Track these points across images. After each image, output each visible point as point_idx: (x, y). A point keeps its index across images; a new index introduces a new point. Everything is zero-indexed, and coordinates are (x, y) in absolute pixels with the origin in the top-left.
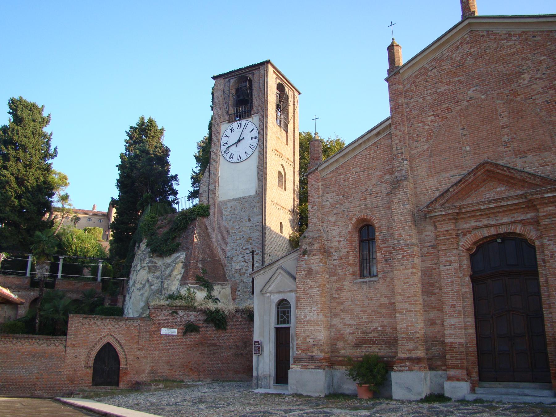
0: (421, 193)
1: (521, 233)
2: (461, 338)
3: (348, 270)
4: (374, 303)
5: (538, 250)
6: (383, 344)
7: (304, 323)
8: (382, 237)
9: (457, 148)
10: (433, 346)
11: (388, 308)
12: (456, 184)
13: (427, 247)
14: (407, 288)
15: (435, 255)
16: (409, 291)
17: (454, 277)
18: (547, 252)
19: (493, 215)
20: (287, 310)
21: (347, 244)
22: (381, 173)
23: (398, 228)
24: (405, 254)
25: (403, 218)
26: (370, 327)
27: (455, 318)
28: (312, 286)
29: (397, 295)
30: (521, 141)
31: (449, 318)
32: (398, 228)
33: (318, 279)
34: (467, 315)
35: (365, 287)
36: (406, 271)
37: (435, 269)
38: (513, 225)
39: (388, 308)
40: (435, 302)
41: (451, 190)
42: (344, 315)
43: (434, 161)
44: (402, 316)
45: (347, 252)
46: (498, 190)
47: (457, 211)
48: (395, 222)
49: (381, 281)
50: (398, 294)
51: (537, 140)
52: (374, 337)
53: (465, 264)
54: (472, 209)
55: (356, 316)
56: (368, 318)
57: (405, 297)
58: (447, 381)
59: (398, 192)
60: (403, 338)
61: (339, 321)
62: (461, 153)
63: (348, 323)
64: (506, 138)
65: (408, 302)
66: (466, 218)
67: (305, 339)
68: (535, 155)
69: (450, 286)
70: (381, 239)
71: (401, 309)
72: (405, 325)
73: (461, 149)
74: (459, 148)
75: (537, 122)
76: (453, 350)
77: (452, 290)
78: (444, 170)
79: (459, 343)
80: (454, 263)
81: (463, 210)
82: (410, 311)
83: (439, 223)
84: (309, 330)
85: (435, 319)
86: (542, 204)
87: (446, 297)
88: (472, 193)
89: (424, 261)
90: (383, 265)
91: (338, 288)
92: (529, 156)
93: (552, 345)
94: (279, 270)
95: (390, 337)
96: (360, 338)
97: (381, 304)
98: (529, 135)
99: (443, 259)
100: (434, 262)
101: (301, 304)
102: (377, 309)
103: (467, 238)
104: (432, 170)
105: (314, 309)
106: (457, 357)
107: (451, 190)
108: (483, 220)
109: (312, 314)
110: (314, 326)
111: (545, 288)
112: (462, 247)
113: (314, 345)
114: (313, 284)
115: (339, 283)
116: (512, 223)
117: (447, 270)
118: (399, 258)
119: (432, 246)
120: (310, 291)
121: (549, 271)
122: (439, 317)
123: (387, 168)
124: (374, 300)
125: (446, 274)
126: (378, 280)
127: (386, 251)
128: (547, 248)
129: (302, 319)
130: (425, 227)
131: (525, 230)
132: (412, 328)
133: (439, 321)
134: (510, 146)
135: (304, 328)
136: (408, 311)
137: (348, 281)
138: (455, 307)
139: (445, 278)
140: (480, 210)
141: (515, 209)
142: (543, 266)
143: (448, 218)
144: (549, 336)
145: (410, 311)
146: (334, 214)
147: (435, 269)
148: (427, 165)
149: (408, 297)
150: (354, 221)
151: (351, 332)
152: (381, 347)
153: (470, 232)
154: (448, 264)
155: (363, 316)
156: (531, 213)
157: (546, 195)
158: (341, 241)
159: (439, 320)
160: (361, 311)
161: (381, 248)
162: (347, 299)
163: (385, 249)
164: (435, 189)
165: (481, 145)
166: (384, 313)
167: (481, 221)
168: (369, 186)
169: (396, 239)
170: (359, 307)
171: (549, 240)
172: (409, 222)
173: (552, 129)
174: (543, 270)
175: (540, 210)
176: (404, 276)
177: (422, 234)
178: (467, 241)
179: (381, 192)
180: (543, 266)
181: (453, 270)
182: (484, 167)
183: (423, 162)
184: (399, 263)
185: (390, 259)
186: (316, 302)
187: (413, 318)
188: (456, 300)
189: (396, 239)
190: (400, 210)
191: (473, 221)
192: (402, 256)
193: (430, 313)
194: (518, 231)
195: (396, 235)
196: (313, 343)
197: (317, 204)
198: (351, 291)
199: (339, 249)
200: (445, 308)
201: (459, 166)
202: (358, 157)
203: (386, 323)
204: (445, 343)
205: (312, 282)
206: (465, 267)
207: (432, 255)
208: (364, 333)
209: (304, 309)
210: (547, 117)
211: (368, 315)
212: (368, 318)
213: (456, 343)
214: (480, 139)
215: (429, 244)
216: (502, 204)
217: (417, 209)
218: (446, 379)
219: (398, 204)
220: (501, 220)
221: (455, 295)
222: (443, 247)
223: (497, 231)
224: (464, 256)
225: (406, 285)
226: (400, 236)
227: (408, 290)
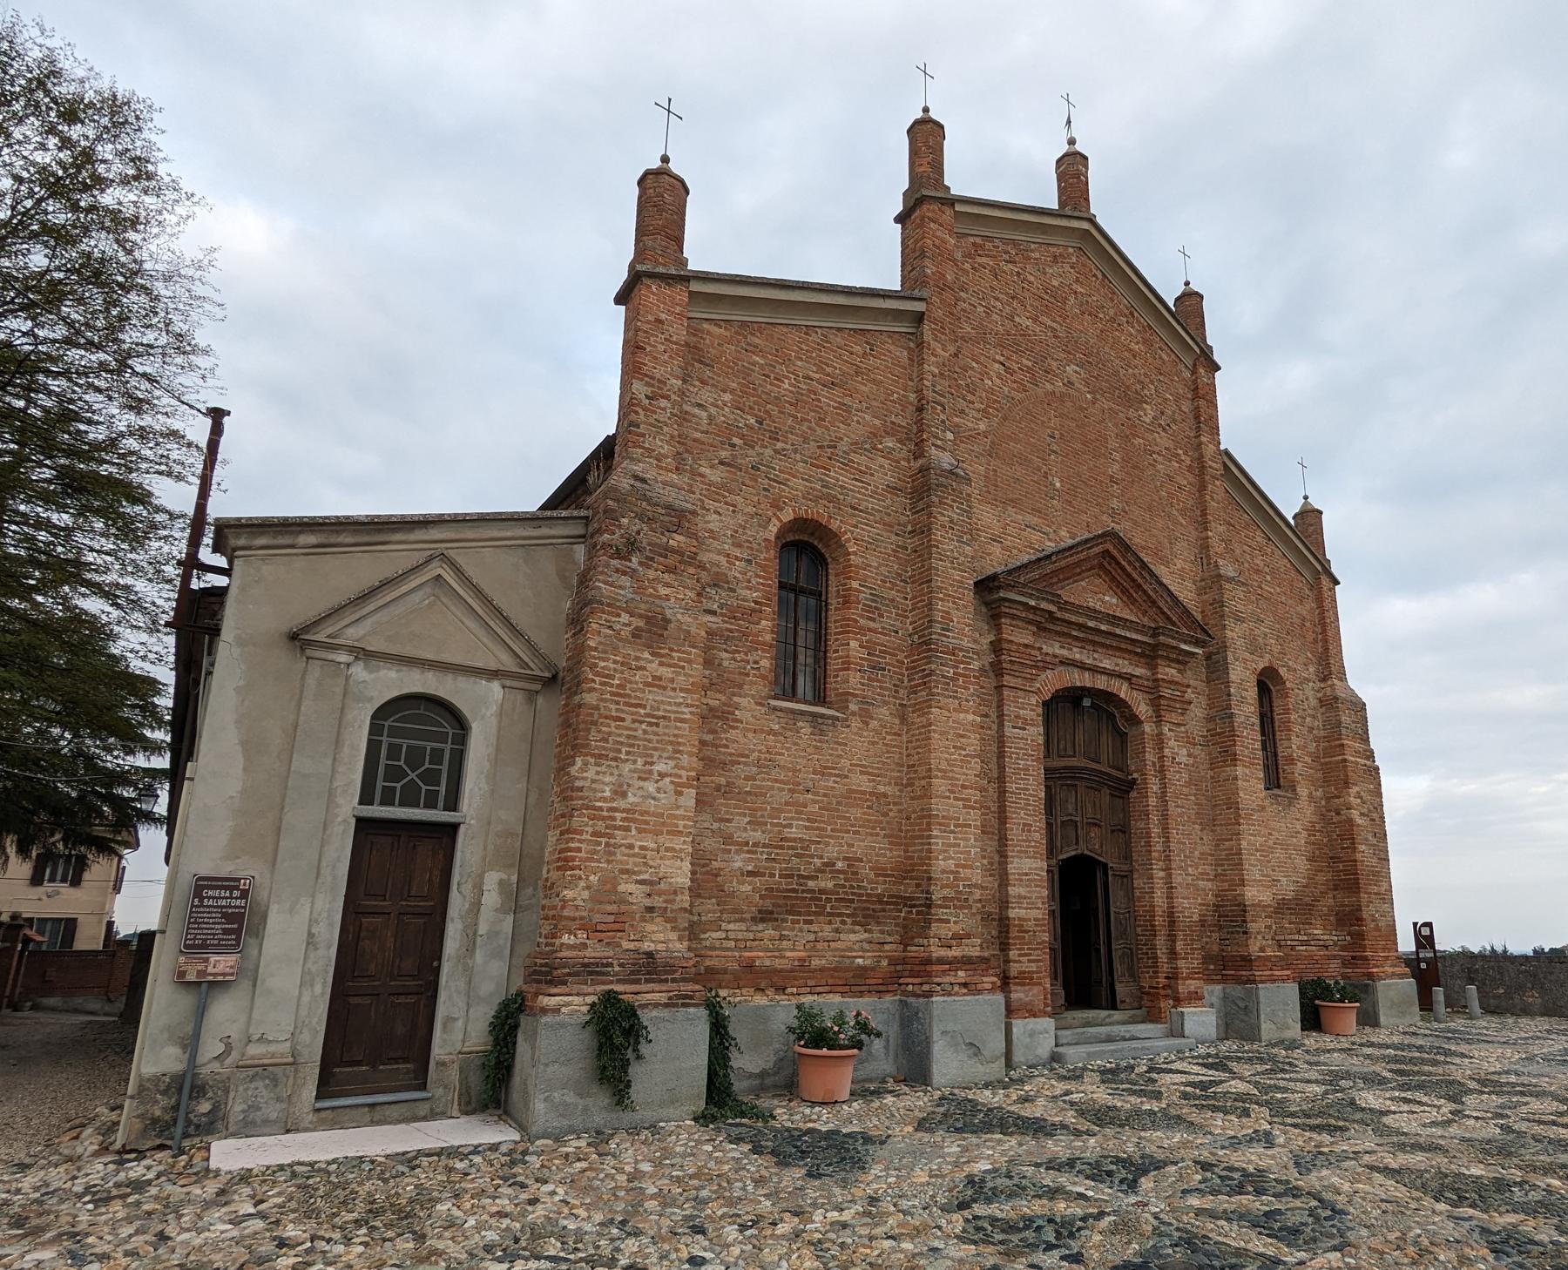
3: (756, 662)
4: (831, 784)
6: (848, 916)
7: (614, 819)
8: (866, 599)
11: (869, 807)
20: (429, 745)
21: (757, 576)
22: (877, 422)
23: (945, 595)
26: (812, 856)
28: (660, 679)
29: (937, 777)
32: (945, 595)
33: (690, 662)
35: (805, 728)
36: (962, 716)
39: (869, 807)
41: (1054, 558)
42: (727, 806)
45: (756, 603)
49: (855, 723)
52: (821, 891)
54: (1073, 618)
55: (771, 817)
56: (807, 828)
57: (956, 785)
61: (706, 825)
63: (739, 836)
64: (1115, 503)
65: (962, 799)
66: (1050, 631)
67: (609, 884)
70: (864, 605)
71: (943, 817)
80: (1032, 725)
84: (631, 847)
90: (863, 677)
91: (711, 709)
94: (436, 569)
95: (868, 895)
96: (778, 890)
97: (851, 791)
101: (605, 740)
102: (838, 803)
105: (660, 767)
108: (1075, 649)
109: (651, 787)
110: (657, 833)
113: (650, 909)
114: (666, 672)
115: (718, 696)
116: (1120, 676)
120: (651, 697)
123: (893, 418)
124: (831, 775)
126: (847, 720)
127: (875, 643)
129: (604, 799)
135: (611, 836)
136: (959, 826)
137: (753, 697)
138: (1029, 831)
140: (1082, 627)
146: (721, 463)
150: (787, 515)
151: (750, 868)
152: (843, 922)
155: (792, 819)
157: (1183, 647)
158: (737, 558)
160: (787, 804)
161: (861, 628)
162: (742, 756)
163: (869, 636)
166: (856, 819)
168: (842, 439)
170: (783, 790)
175: (1160, 669)
176: (956, 728)
186: (671, 743)
189: (939, 622)
191: (1057, 645)
195: (939, 611)
196: (648, 902)
197: (673, 397)
198: (762, 731)
199: (728, 583)
202: (814, 337)
203: (859, 850)
205: (661, 664)
208: (792, 876)
209: (615, 759)
211: (808, 820)
212: (807, 828)
216: (1118, 631)
220: (1101, 661)
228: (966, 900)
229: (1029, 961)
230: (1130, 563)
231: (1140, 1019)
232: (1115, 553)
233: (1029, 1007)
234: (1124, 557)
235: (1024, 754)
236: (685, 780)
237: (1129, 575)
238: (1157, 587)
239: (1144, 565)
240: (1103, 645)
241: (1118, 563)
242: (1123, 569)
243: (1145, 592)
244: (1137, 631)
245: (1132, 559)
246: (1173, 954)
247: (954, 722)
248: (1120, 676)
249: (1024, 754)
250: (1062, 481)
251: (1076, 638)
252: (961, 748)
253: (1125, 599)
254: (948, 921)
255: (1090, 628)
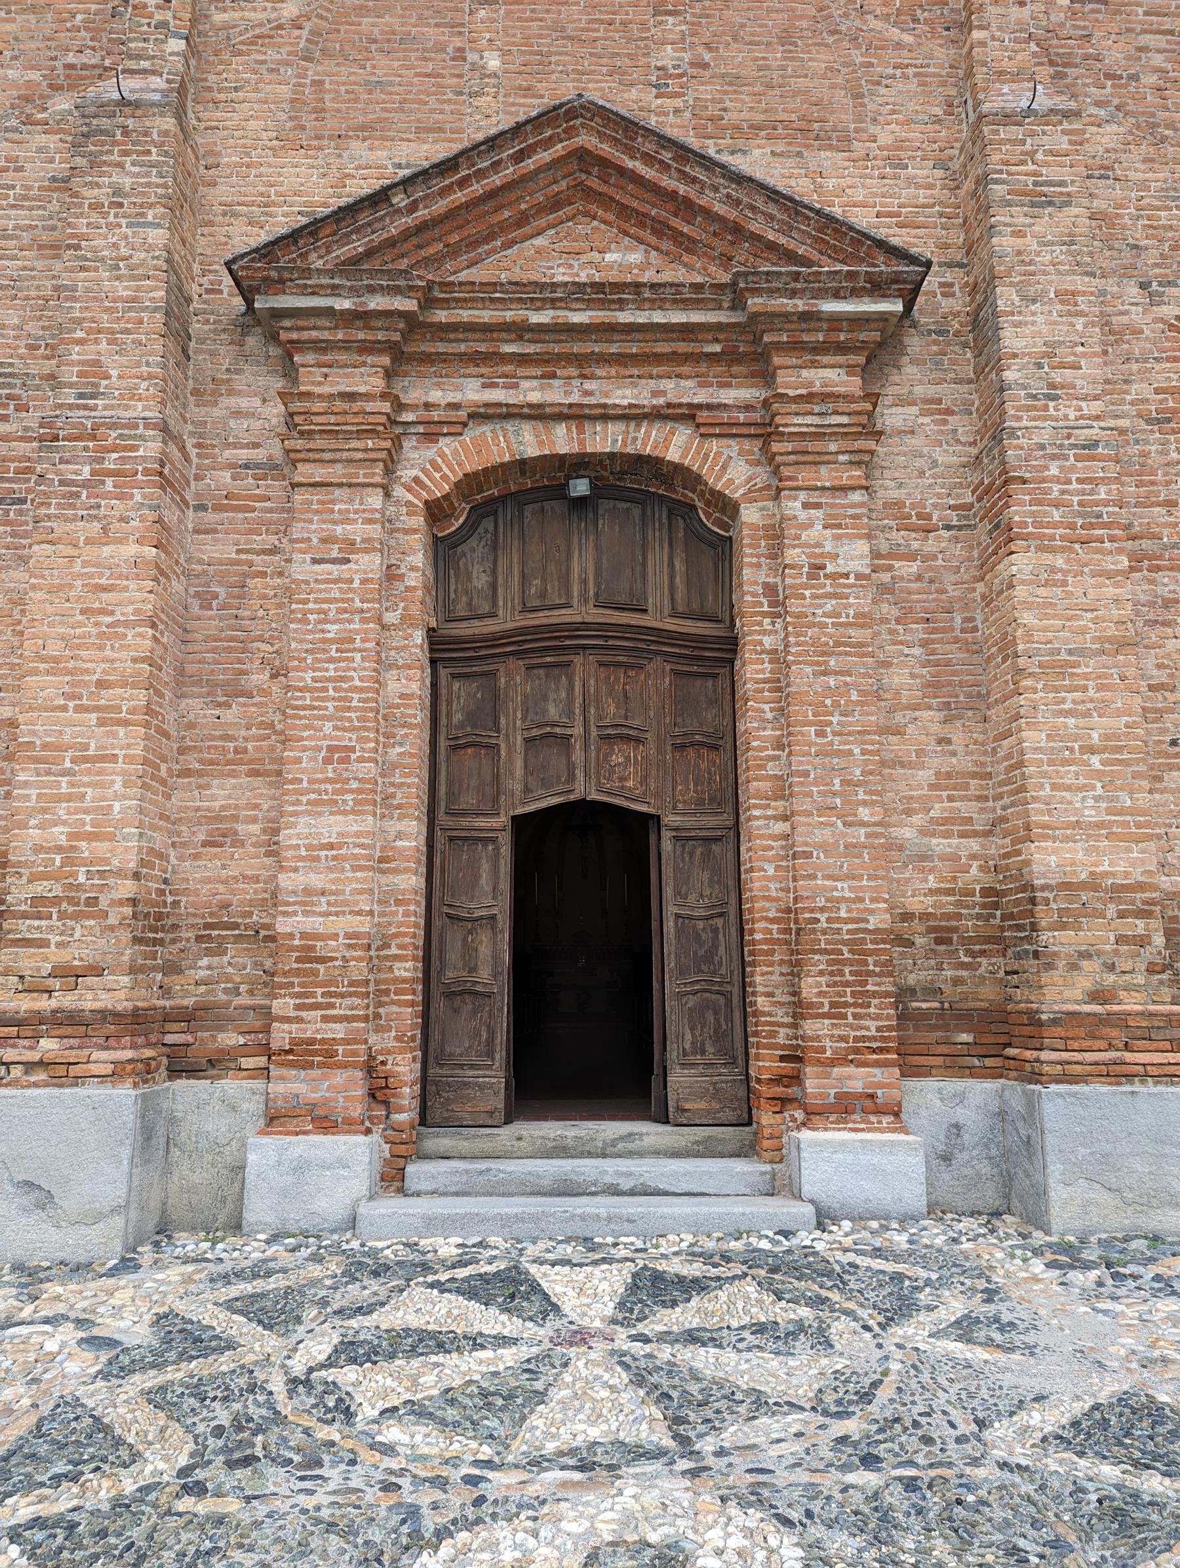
0: (235, 215)
1: (686, 462)
2: (359, 913)
5: (751, 546)
9: (443, 50)
10: (209, 952)
12: (423, 175)
13: (232, 466)
14: (100, 635)
15: (271, 511)
16: (108, 653)
17: (357, 618)
18: (793, 555)
19: (572, 371)
22: (35, 76)
24: (111, 461)
25: (123, 290)
27: (345, 813)
29: (35, 672)
30: (730, 84)
31: (309, 813)
34: (399, 807)
36: (106, 551)
37: (263, 574)
38: (657, 425)
40: (243, 733)
41: (400, 200)
43: (320, 83)
44: (43, 785)
46: (609, 257)
47: (409, 304)
48: (75, 299)
50: (42, 666)
51: (795, 94)
53: (412, 569)
54: (486, 316)
57: (85, 684)
58: (262, 1133)
59: (115, 157)
60: (37, 900)
62: (460, 76)
64: (667, 56)
65: (97, 709)
66: (443, 358)
68: (781, 155)
69: (331, 660)
71: (45, 746)
72: (59, 833)
73: (460, 55)
74: (450, 50)
75: (805, 24)
76: (315, 973)
77: (342, 679)
78: (366, 131)
79: (348, 936)
80: (366, 551)
81: (442, 316)
82: (104, 758)
83: (310, 358)
85: (235, 818)
86: (796, 347)
87: (304, 708)
88: (494, 251)
89: (207, 532)
92: (757, 152)
93: (777, 957)
98: (768, 68)
99: (311, 528)
100: (261, 540)
103: (442, 455)
104: (308, 120)
106: (332, 1006)
107: (400, 200)
108: (525, 384)
111: (766, 707)
112: (409, 490)
116: (657, 415)
117: (327, 581)
118: (72, 483)
119: (258, 466)
121: (798, 635)
122: (256, 806)
123: (71, 58)
125: (316, 601)
128: (798, 537)
130: (238, 372)
131: (707, 456)
132: (102, 847)
133: (255, 828)
134: (684, 95)
136: (86, 759)
138: (345, 760)
139: (311, 617)
140: (520, 330)
141: (674, 358)
142: (764, 615)
143: (361, 336)
144: (767, 919)
145: (104, 758)
147: (263, 574)
148: (285, 91)
149: (101, 684)
153: (457, 428)
154: (335, 554)
156: (739, 386)
157: (830, 306)
159: (254, 820)
164: (305, 204)
165: (553, 59)
167: (516, 386)
169: (71, 385)
171: (806, 506)
172: (150, 377)
173: (863, 65)
174: (764, 632)
175: (782, 377)
176: (91, 576)
177: (216, 403)
178: (438, 469)
179: (19, 169)
180: (764, 615)
181: (356, 584)
182: (570, 132)
183: (268, 76)
184: (72, 506)
185: (23, 501)
187: (117, 797)
188: (353, 729)
189: (71, 385)
190: (115, 246)
192: (93, 473)
193: (207, 786)
194: (673, 455)
195: (72, 363)
200: (299, 760)
201: (441, 130)
204: (272, 939)
206: (413, 580)
207: (254, 510)
210: (846, 15)
213: (335, 936)
214: (554, 35)
215: (244, 454)
217: (204, 280)
218: (262, 1122)
219: (105, 215)
221: (355, 703)
222: (319, 473)
223: (582, 442)
224: (415, 531)
225: (97, 624)
226: (95, 369)
227: (101, 648)
228: (92, 901)
229: (326, 1019)
230: (648, 159)
231: (730, 1148)
232: (606, 149)
233: (320, 1112)
234: (631, 152)
235: (341, 611)
236: (305, 784)
237: (654, 188)
238: (733, 190)
239: (684, 152)
240: (604, 359)
241: (622, 171)
242: (637, 179)
243: (706, 212)
244: (684, 304)
245: (649, 147)
246: (799, 1009)
247: (85, 564)
248: (657, 415)
249: (341, 611)
250: (505, 53)
251: (522, 360)
252: (103, 612)
253: (666, 245)
254: (44, 943)
255: (541, 328)
